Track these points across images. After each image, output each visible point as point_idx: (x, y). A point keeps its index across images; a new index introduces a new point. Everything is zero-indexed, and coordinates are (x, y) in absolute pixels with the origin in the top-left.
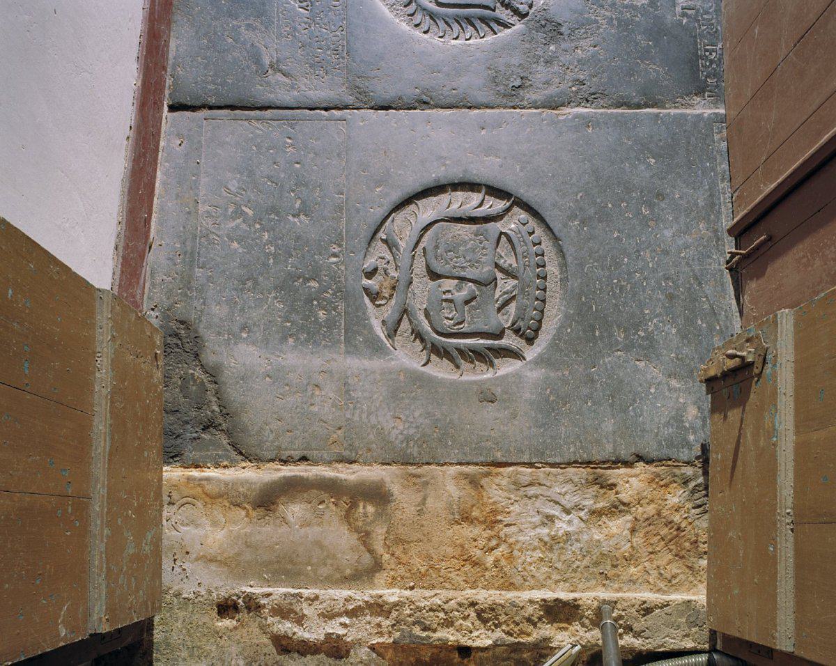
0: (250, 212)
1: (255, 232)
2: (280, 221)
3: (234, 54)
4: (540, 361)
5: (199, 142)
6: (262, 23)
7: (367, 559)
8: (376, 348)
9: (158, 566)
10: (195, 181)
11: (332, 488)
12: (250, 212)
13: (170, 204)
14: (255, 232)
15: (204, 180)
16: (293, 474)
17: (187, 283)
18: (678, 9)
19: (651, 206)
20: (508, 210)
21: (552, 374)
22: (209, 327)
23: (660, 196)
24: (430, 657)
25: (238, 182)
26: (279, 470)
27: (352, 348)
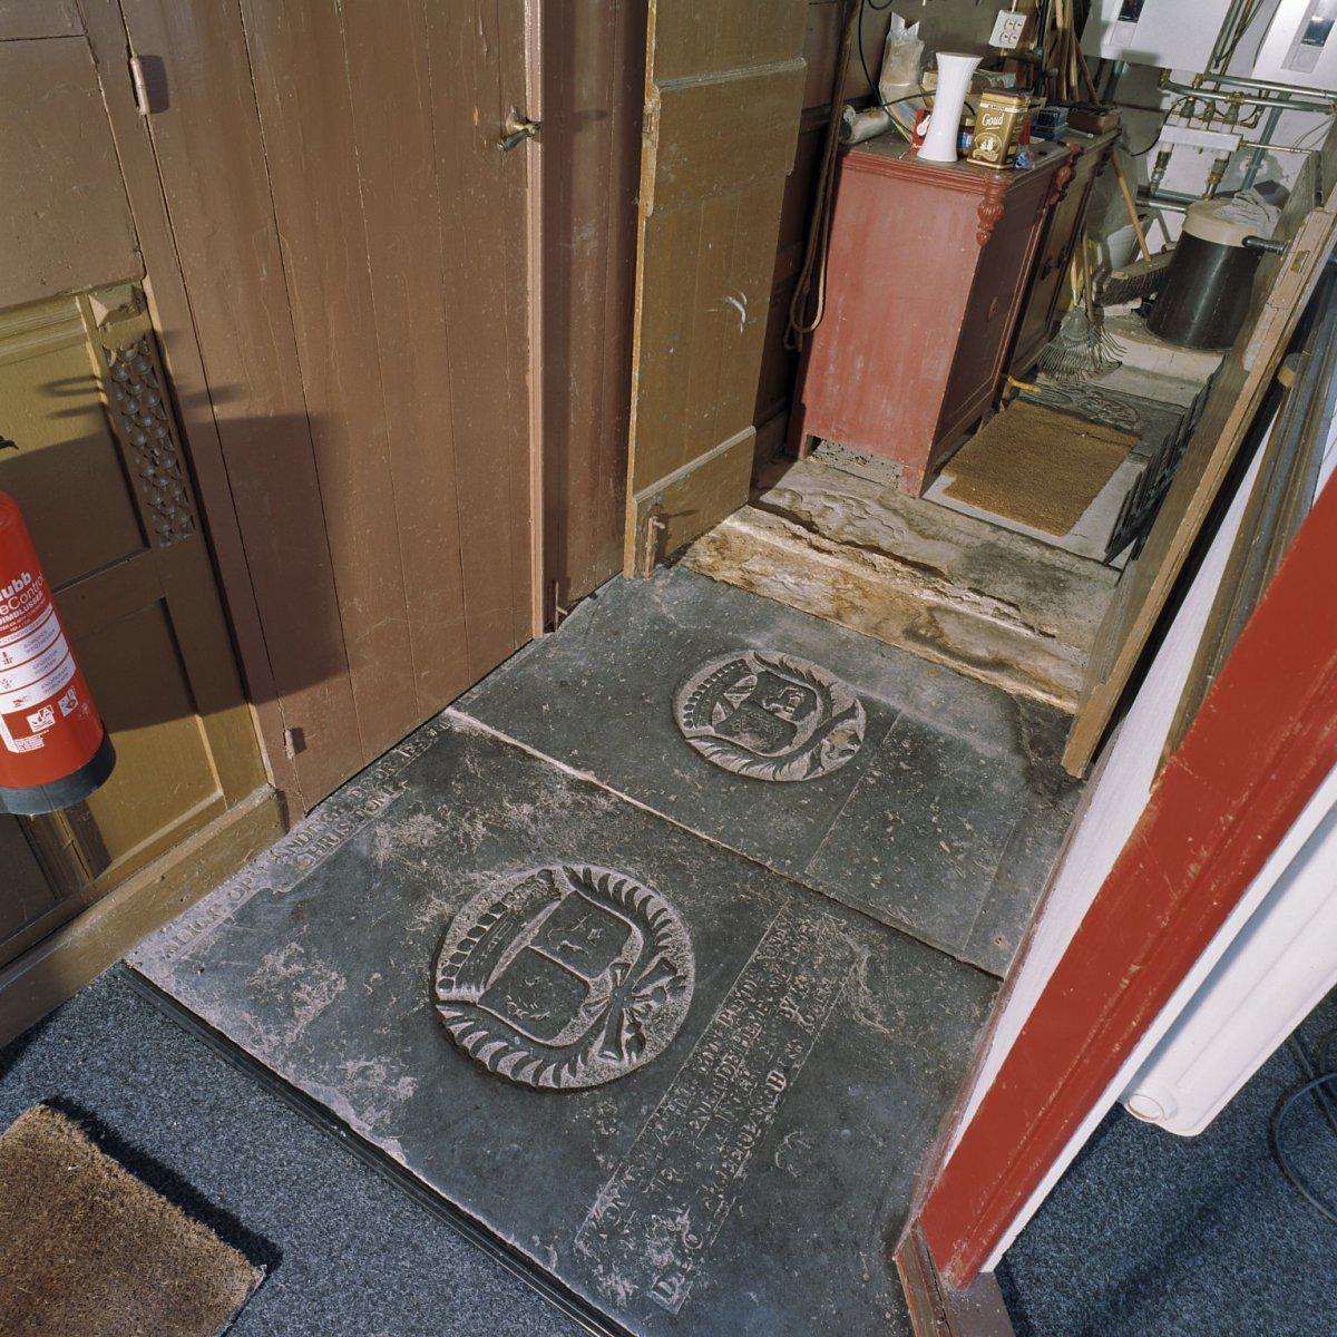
0: (943, 844)
1: (945, 826)
2: (916, 823)
3: (901, 995)
4: (745, 647)
5: (976, 931)
6: (853, 1012)
7: (1122, 568)
8: (869, 705)
9: (732, 592)
10: (993, 896)
11: (944, 649)
12: (943, 844)
13: (1027, 890)
14: (945, 826)
15: (983, 895)
16: (975, 669)
17: (1026, 818)
18: (396, 795)
19: (577, 683)
20: (691, 738)
21: (742, 637)
22: (1014, 781)
23: (563, 684)
24: (595, 1199)
25: (945, 875)
26: (984, 676)
27: (892, 714)
